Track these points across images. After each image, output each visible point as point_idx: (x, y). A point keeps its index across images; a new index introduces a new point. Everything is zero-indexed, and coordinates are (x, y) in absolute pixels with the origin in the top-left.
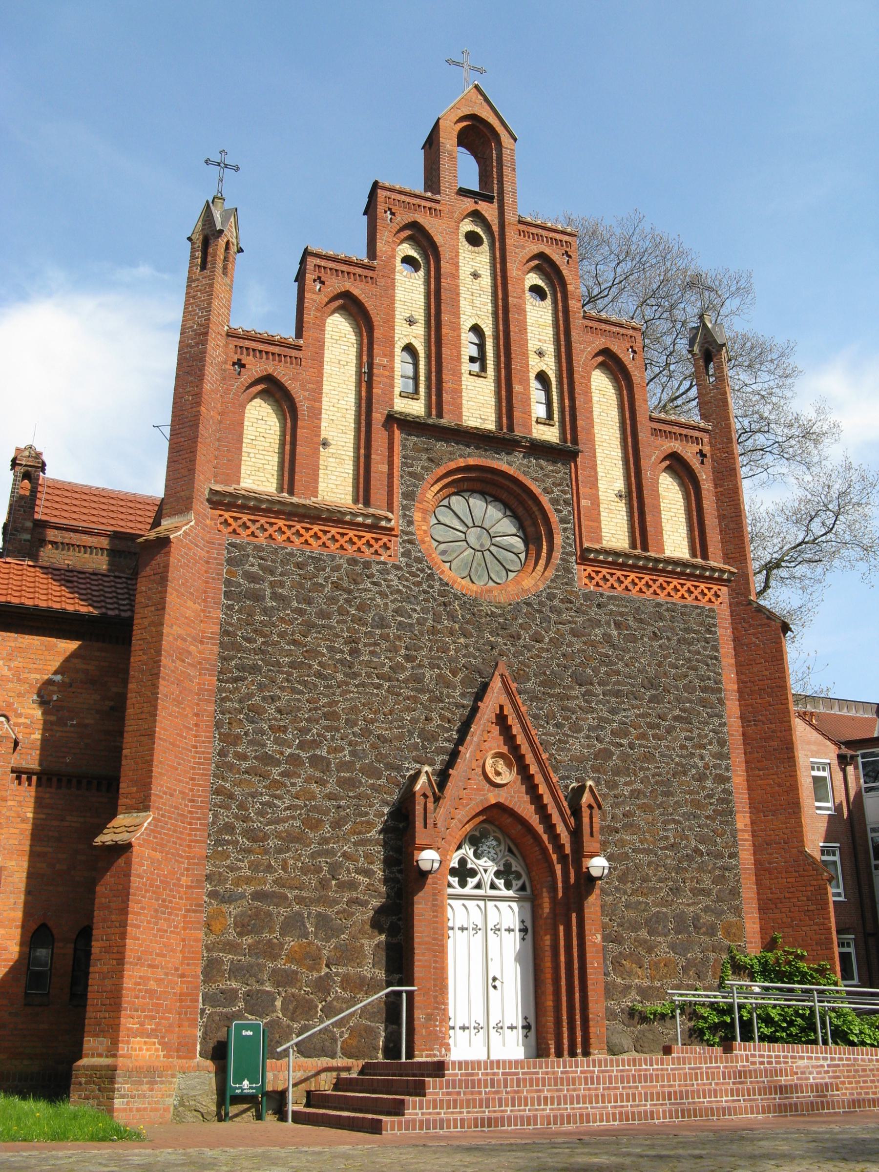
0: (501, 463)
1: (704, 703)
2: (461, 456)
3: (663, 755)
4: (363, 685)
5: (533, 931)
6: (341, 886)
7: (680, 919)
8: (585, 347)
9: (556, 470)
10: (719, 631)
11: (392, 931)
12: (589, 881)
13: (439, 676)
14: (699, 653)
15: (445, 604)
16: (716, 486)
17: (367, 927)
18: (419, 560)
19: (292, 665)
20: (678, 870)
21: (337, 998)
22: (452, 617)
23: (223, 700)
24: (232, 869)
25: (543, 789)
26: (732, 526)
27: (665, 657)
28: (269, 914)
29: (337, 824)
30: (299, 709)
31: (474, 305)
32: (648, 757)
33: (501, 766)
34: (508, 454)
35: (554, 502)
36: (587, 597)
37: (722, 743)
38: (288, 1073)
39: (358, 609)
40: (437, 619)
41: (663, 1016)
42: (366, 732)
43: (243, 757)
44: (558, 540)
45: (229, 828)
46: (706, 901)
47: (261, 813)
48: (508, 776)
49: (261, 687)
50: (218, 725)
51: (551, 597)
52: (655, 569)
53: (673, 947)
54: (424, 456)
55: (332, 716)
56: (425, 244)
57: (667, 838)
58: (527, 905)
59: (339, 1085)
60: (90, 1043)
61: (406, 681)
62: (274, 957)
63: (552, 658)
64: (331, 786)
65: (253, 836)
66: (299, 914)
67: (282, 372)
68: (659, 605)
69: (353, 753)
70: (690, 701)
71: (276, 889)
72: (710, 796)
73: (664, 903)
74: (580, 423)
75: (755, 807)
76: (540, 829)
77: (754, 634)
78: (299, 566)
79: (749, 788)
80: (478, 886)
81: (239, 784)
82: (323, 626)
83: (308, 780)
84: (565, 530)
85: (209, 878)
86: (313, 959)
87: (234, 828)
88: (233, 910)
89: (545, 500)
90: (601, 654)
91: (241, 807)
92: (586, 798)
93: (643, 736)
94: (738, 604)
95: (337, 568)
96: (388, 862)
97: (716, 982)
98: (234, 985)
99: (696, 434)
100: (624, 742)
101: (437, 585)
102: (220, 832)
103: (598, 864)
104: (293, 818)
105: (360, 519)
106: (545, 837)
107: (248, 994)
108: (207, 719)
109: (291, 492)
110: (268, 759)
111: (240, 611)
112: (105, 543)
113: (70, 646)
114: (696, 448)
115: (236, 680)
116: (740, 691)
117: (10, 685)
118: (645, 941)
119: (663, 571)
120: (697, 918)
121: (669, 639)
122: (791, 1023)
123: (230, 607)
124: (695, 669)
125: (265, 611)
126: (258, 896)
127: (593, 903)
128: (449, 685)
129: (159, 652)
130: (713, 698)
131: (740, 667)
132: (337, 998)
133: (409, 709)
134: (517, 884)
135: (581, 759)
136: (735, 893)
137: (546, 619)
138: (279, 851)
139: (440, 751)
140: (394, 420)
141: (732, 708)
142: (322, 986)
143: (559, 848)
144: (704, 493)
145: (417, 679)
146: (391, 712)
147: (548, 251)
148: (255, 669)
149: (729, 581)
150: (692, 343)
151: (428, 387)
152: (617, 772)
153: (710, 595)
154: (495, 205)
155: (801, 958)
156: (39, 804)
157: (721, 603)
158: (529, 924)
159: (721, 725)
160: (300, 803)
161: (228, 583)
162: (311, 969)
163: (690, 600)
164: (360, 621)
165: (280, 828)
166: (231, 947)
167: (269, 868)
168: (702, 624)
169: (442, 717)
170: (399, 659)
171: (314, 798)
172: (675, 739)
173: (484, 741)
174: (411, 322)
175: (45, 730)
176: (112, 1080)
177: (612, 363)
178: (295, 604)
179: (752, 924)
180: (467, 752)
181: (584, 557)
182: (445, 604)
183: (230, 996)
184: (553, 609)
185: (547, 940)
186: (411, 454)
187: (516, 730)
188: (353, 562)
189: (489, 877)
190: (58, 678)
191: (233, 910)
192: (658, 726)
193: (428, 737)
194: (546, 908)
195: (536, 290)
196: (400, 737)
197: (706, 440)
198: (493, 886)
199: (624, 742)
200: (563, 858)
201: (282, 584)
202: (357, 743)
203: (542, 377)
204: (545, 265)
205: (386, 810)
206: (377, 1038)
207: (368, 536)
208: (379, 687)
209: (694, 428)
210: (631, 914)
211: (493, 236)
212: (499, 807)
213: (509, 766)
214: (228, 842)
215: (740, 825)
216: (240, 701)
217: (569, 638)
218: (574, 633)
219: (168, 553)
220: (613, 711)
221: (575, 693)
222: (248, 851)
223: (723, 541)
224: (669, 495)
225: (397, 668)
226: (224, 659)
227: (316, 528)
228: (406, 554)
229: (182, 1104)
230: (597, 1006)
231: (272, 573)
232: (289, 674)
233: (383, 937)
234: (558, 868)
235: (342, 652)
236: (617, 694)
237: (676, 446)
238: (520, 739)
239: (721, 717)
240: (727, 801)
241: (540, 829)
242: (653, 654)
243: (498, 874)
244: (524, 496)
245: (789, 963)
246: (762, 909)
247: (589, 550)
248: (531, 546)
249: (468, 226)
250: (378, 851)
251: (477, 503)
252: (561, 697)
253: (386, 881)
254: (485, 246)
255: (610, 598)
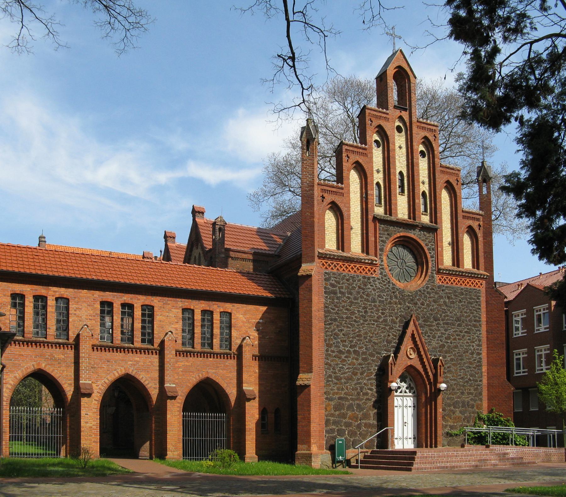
0: (412, 234)
1: (475, 326)
2: (398, 232)
3: (461, 346)
4: (369, 324)
5: (417, 407)
6: (364, 394)
7: (463, 402)
8: (441, 180)
9: (430, 236)
10: (482, 299)
11: (378, 409)
12: (440, 390)
13: (392, 319)
14: (474, 307)
15: (394, 292)
16: (484, 239)
17: (371, 407)
18: (385, 276)
19: (347, 318)
20: (464, 386)
21: (363, 430)
22: (396, 297)
23: (326, 331)
24: (332, 390)
25: (425, 360)
26: (489, 256)
27: (463, 309)
28: (343, 404)
29: (362, 374)
30: (350, 334)
31: (400, 164)
32: (456, 347)
33: (412, 352)
34: (414, 230)
35: (429, 249)
36: (439, 287)
37: (480, 341)
38: (350, 453)
39: (367, 296)
40: (391, 298)
41: (457, 435)
42: (370, 341)
43: (333, 352)
44: (430, 265)
45: (330, 376)
46: (471, 397)
47: (339, 371)
48: (413, 356)
49: (338, 326)
50: (325, 340)
51: (427, 288)
52: (462, 275)
53: (461, 412)
54: (386, 233)
55: (359, 336)
56: (383, 134)
57: (461, 375)
58: (415, 398)
59: (365, 457)
60: (299, 446)
61: (382, 322)
62: (345, 418)
63: (427, 311)
64: (360, 361)
65: (336, 378)
66: (352, 404)
67: (338, 200)
68: (462, 289)
69: (366, 349)
70: (470, 326)
71: (345, 396)
72: (475, 360)
73: (459, 397)
74: (438, 215)
75: (489, 364)
76: (423, 373)
77: (494, 300)
78: (348, 280)
79: (487, 357)
80: (401, 392)
81: (332, 361)
82: (356, 303)
83: (352, 359)
84: (432, 261)
85: (325, 393)
86: (355, 418)
87: (332, 376)
88: (333, 403)
89: (426, 249)
90: (443, 309)
91: (334, 369)
92: (439, 363)
93: (455, 339)
94: (489, 288)
95: (359, 280)
96: (378, 386)
97: (473, 424)
98: (334, 427)
99: (478, 217)
100: (449, 341)
101: (391, 286)
102: (328, 377)
103: (443, 386)
104: (349, 372)
105: (367, 261)
106: (425, 376)
107: (338, 430)
108: (322, 339)
109: (343, 250)
110: (340, 352)
111: (330, 298)
112: (251, 257)
113: (264, 309)
114: (477, 223)
115: (330, 324)
116: (487, 321)
117: (246, 324)
118: (453, 410)
119: (465, 276)
120: (468, 402)
121: (465, 302)
122: (497, 437)
123: (326, 297)
124: (472, 313)
125: (338, 298)
126: (340, 398)
127: (440, 399)
128: (395, 323)
129: (311, 317)
130: (478, 324)
131: (488, 312)
132: (363, 430)
133: (383, 332)
134: (412, 391)
135: (435, 348)
136: (480, 394)
137: (425, 296)
138: (345, 383)
139: (393, 347)
140: (375, 219)
141: (484, 328)
142: (359, 427)
143: (429, 379)
144: (479, 242)
145: (385, 321)
146: (377, 334)
147: (428, 135)
148: (335, 320)
149: (486, 278)
150: (478, 176)
151: (385, 201)
152: (446, 352)
153: (479, 284)
154: (408, 112)
155: (501, 416)
156: (260, 367)
157: (482, 287)
158: (416, 404)
159: (480, 334)
160: (351, 367)
161: (325, 288)
162: (356, 421)
163: (472, 287)
164: (367, 300)
165: (345, 375)
166: (332, 415)
167: (343, 389)
168: (476, 296)
169: (393, 335)
170: (380, 314)
171: (355, 365)
172: (465, 340)
173: (407, 344)
174: (378, 171)
175: (259, 340)
176: (311, 457)
177: (450, 188)
178: (347, 295)
179: (485, 404)
180: (403, 347)
181: (439, 271)
182: (394, 292)
183: (332, 431)
184: (428, 293)
185: (423, 410)
186: (382, 232)
187: (417, 339)
188: (364, 277)
189: (404, 389)
190: (261, 321)
191: (333, 403)
192: (459, 335)
193: (389, 342)
194: (423, 400)
195: (422, 153)
196: (380, 342)
197: (481, 219)
198: (405, 392)
199: (449, 341)
200: (430, 383)
201: (342, 288)
202: (367, 345)
203: (424, 194)
204: (427, 142)
205: (376, 368)
206: (374, 442)
207: (369, 267)
208: (373, 324)
209: (477, 214)
210: (449, 401)
211: (407, 128)
212: (411, 366)
213: (414, 351)
214: (330, 381)
215: (483, 370)
216: (331, 332)
217: (433, 303)
218: (434, 301)
219: (311, 280)
220: (446, 330)
221: (434, 324)
222: (336, 384)
223: (485, 262)
224: (466, 241)
225: (379, 317)
226: (326, 317)
227: (352, 265)
228: (381, 273)
229: (322, 464)
230: (440, 432)
231: (339, 283)
232: (346, 321)
233: (376, 411)
234: (428, 386)
235: (362, 312)
236: (447, 324)
237: (470, 222)
238: (419, 343)
239: (480, 331)
240: (480, 362)
241: (423, 373)
242: (459, 308)
243: (407, 388)
244: (418, 247)
245: (497, 418)
246: (489, 399)
247: (440, 269)
248: (419, 266)
249: (397, 123)
250: (374, 382)
251: (400, 249)
252: (429, 326)
253: (377, 392)
254: (403, 133)
255: (447, 287)
